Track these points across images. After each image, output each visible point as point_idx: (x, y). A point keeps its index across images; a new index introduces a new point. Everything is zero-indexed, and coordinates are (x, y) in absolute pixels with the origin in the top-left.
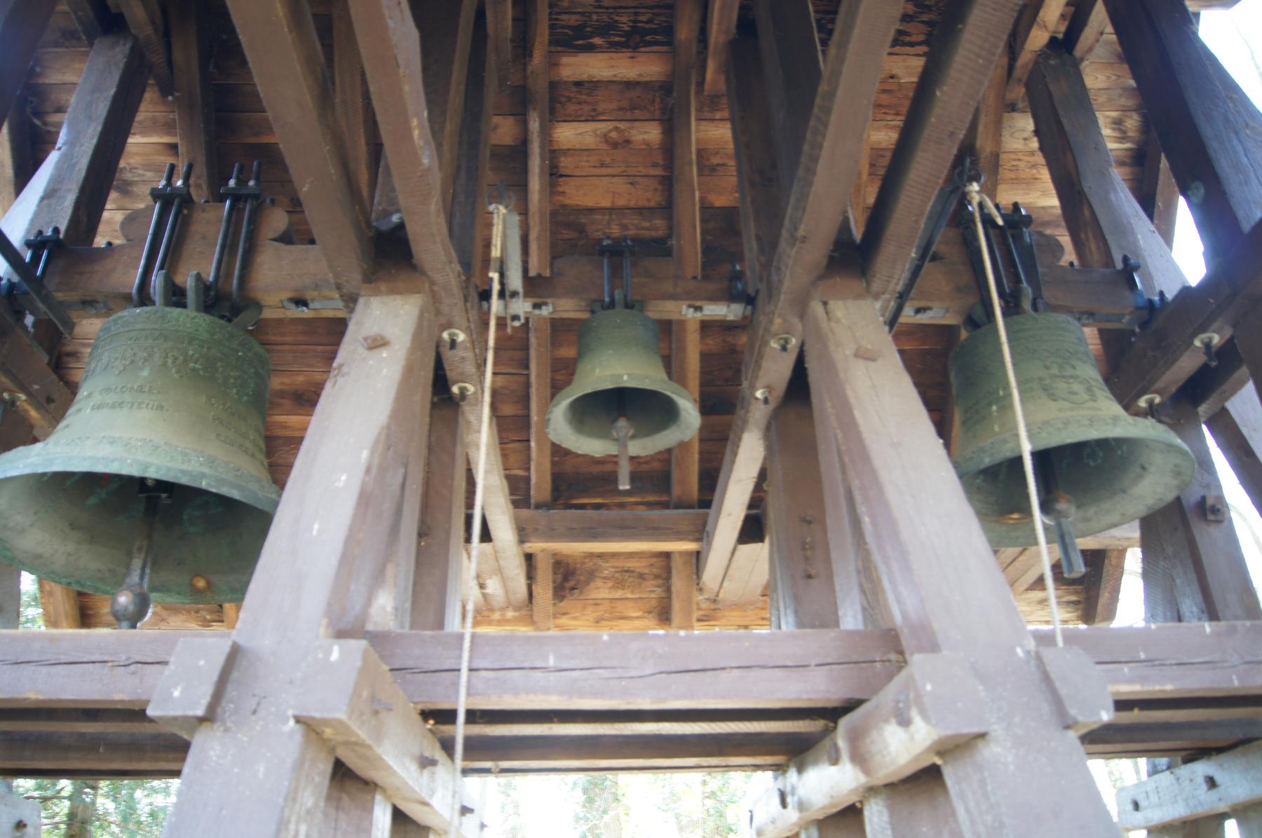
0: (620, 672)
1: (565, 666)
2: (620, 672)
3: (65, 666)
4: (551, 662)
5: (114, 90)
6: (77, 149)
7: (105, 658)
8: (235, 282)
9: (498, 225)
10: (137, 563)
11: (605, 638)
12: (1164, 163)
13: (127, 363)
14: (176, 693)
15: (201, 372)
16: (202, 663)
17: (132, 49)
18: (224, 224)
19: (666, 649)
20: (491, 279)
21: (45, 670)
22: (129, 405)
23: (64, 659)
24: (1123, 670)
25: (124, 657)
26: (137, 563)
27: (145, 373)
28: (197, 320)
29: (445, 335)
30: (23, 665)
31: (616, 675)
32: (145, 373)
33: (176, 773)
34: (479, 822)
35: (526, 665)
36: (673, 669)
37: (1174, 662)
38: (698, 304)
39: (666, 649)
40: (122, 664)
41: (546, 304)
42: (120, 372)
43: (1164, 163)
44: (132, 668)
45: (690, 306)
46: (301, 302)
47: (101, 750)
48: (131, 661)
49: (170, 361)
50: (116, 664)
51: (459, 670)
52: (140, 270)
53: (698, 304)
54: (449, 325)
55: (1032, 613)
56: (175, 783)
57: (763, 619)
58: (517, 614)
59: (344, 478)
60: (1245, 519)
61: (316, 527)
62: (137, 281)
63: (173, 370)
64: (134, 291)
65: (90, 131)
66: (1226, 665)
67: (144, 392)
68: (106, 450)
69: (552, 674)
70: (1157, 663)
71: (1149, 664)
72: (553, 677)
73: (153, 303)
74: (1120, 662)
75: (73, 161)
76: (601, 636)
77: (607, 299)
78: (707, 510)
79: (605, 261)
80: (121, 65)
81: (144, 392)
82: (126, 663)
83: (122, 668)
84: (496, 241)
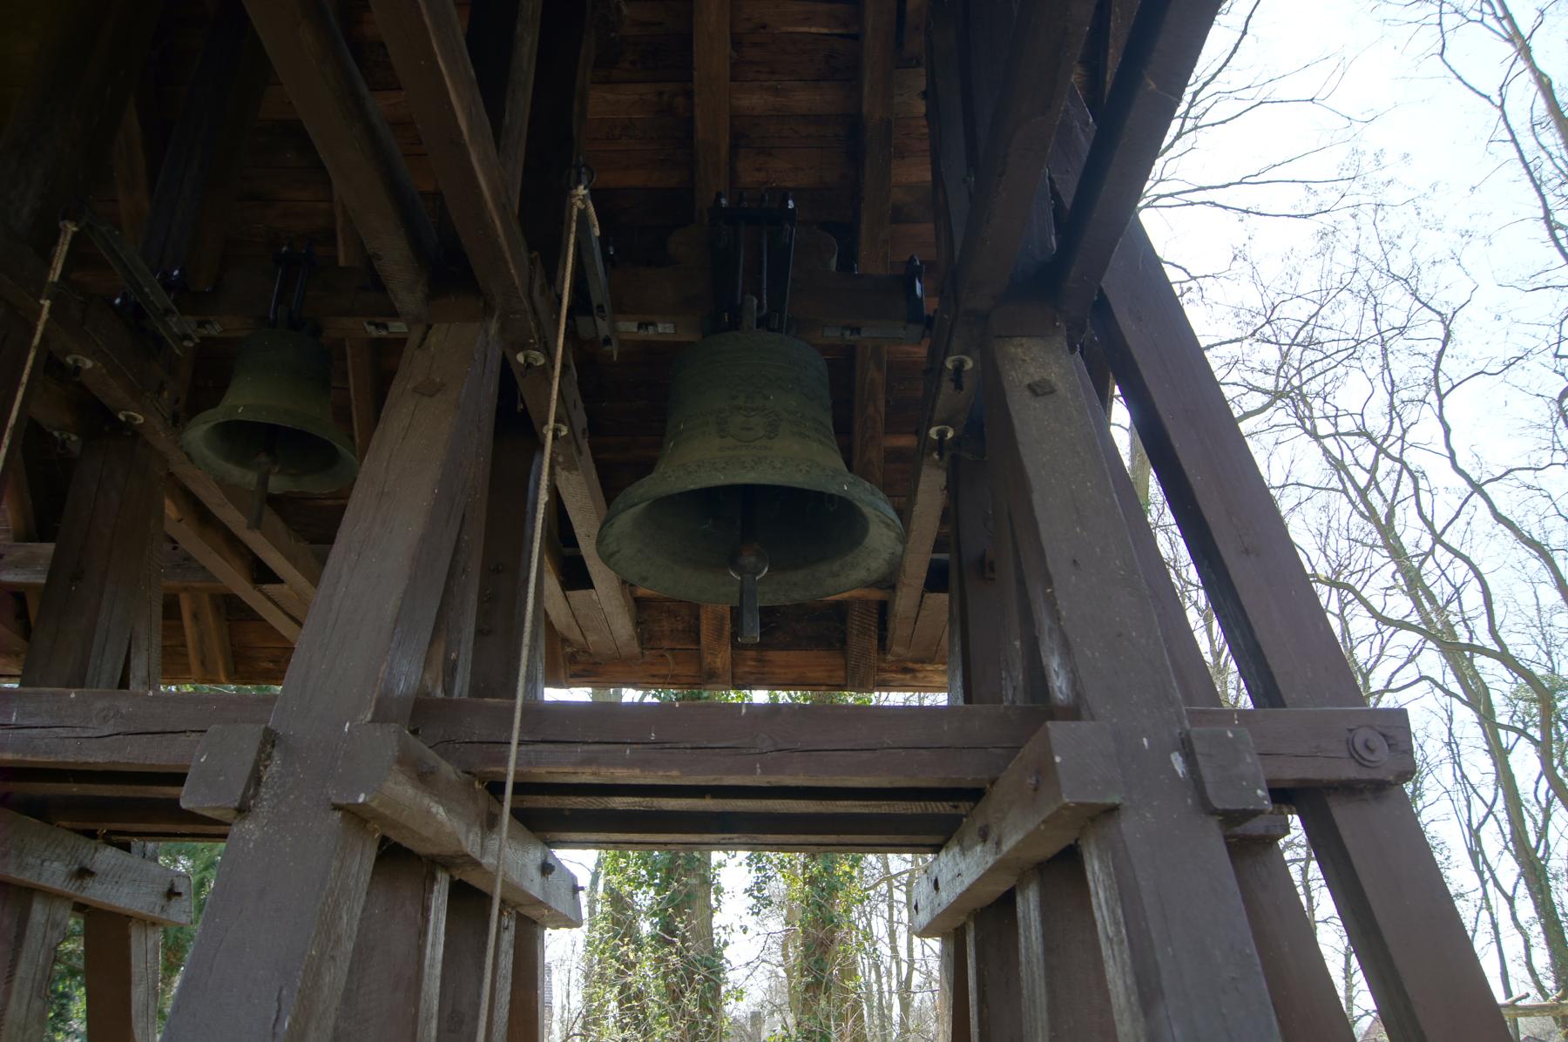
1: (27, 723)
9: (63, 244)
11: (73, 696)
20: (42, 306)
24: (625, 752)
29: (520, 358)
31: (75, 735)
33: (224, 836)
36: (132, 730)
37: (688, 745)
51: (510, 743)
54: (523, 347)
56: (222, 846)
60: (1303, 551)
66: (752, 751)
69: (11, 731)
70: (668, 746)
71: (658, 746)
74: (624, 743)
76: (69, 694)
78: (937, 556)
84: (57, 264)
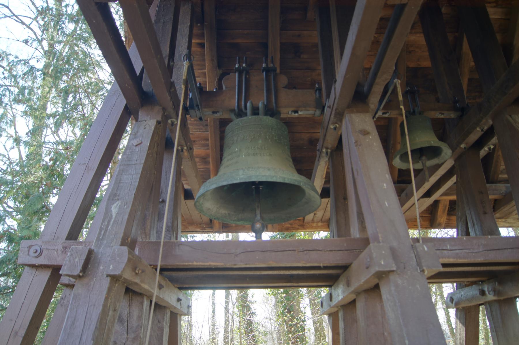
0: (471, 251)
1: (454, 248)
2: (471, 251)
3: (281, 252)
4: (448, 247)
5: (189, 23)
6: (180, 48)
7: (295, 249)
8: (274, 104)
10: (258, 212)
12: (465, 39)
13: (253, 137)
14: (383, 263)
15: (278, 141)
16: (383, 252)
17: (192, 6)
18: (265, 82)
19: (485, 242)
20: (401, 109)
21: (273, 253)
22: (260, 154)
23: (279, 249)
25: (301, 248)
26: (258, 212)
27: (260, 142)
28: (272, 121)
30: (265, 252)
32: (260, 142)
34: (177, 298)
35: (440, 248)
38: (443, 112)
39: (485, 242)
40: (301, 251)
41: (388, 112)
42: (250, 141)
43: (465, 39)
44: (305, 252)
45: (440, 113)
46: (296, 112)
47: (248, 280)
48: (304, 250)
49: (267, 137)
50: (299, 251)
52: (236, 100)
53: (443, 112)
55: (515, 223)
57: (415, 225)
58: (322, 224)
59: (385, 185)
61: (386, 203)
62: (236, 104)
63: (270, 140)
64: (236, 108)
65: (184, 41)
67: (262, 149)
68: (268, 173)
72: (450, 252)
73: (246, 115)
75: (180, 53)
77: (412, 111)
79: (408, 96)
80: (190, 13)
81: (262, 149)
82: (303, 250)
83: (302, 252)
